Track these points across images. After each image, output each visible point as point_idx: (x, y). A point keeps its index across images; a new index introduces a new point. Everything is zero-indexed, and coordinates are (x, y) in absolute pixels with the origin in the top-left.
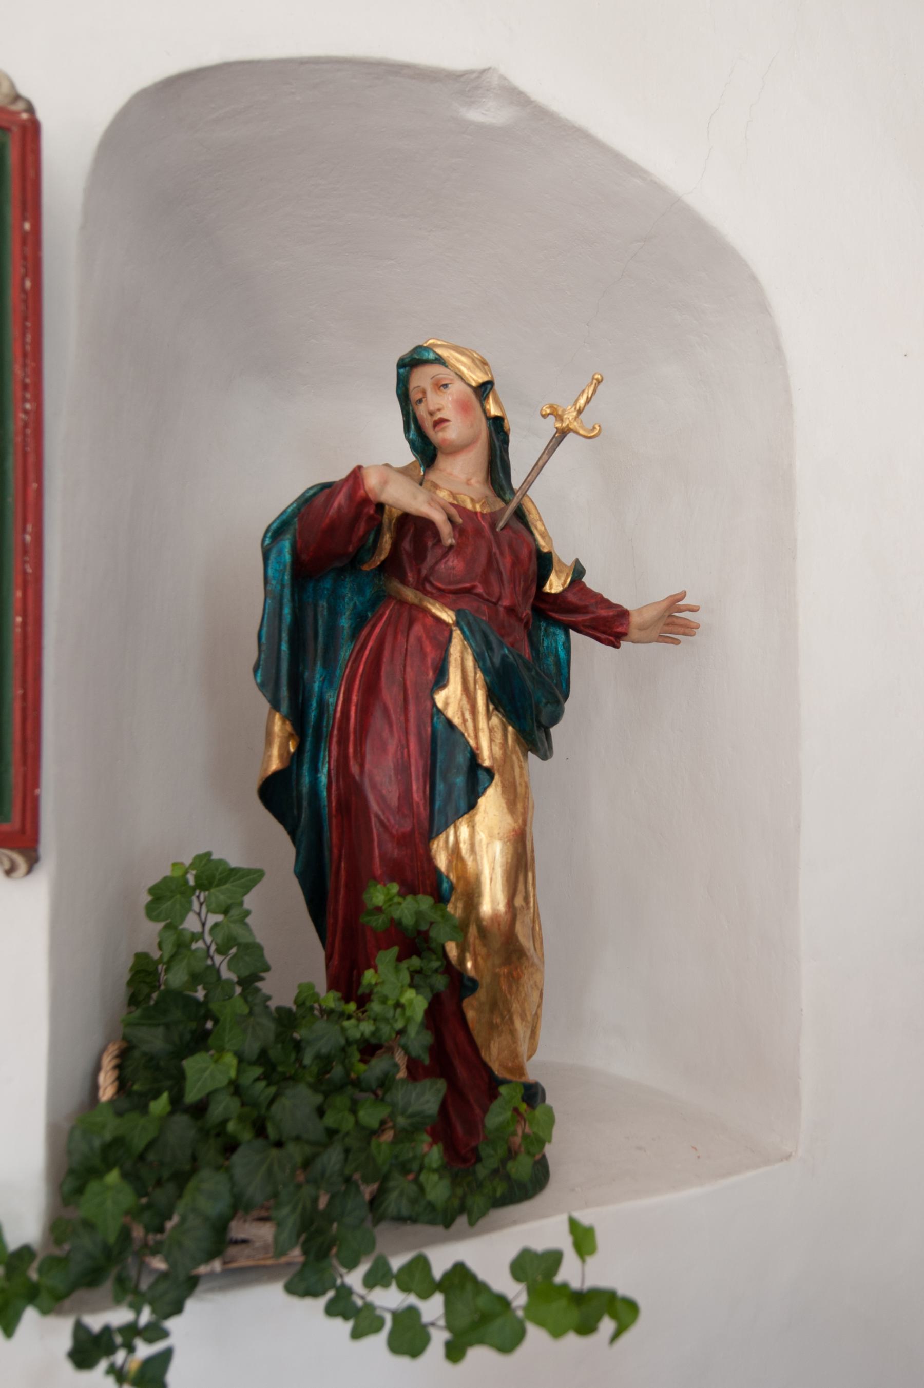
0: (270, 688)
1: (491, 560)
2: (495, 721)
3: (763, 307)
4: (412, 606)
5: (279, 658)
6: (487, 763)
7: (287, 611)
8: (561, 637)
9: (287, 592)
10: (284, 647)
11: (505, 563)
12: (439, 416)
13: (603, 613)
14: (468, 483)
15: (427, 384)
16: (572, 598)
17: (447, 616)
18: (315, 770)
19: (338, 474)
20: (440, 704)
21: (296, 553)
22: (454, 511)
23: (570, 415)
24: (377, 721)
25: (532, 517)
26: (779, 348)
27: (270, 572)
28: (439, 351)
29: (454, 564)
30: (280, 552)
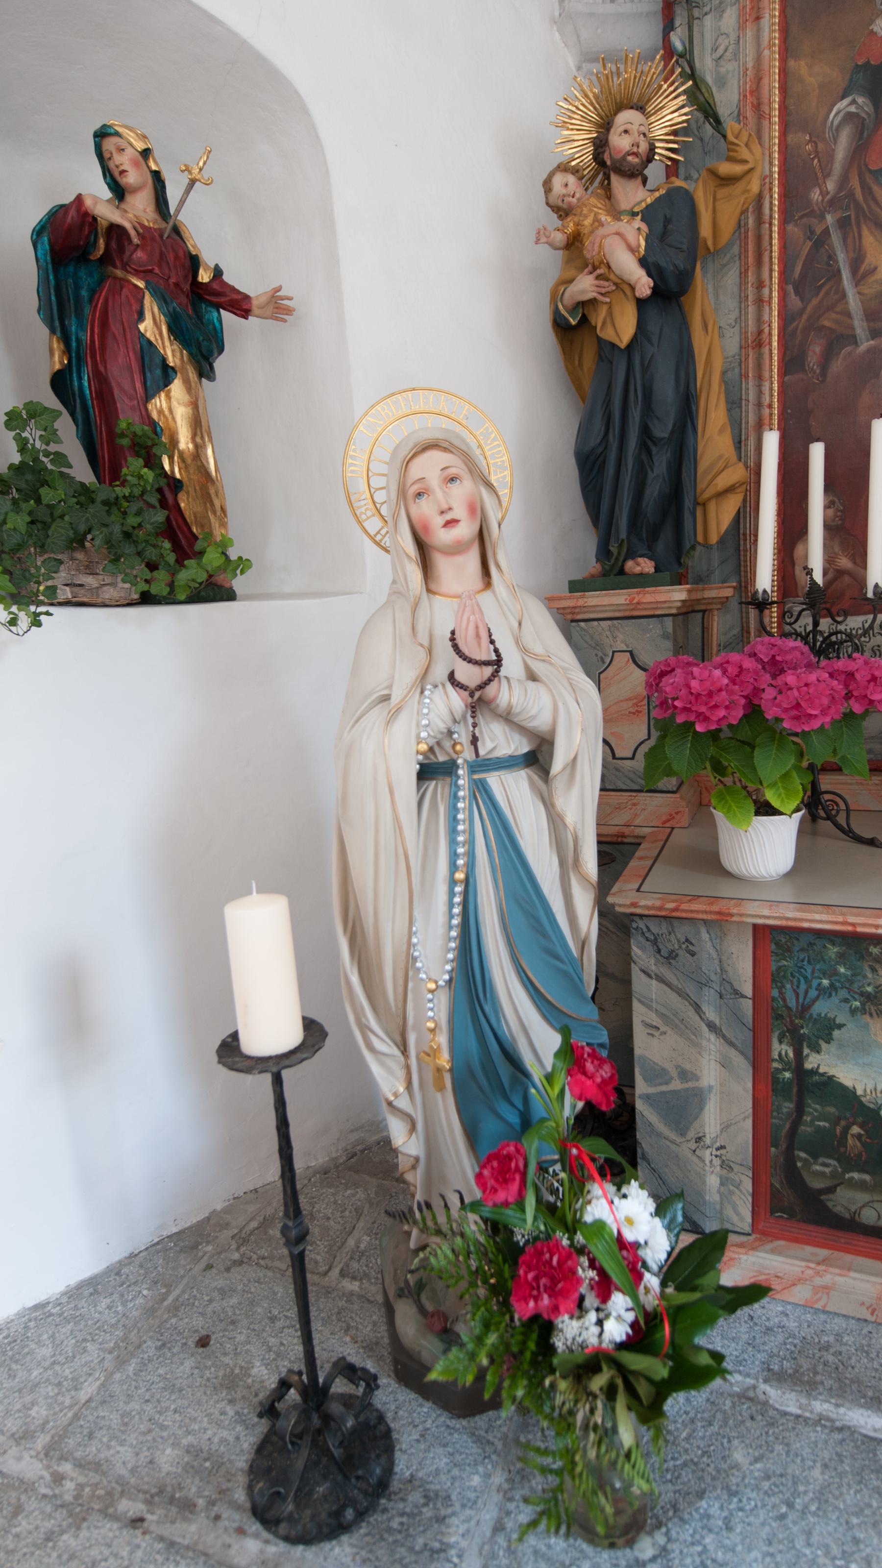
0: (50, 323)
1: (162, 254)
2: (175, 347)
3: (306, 111)
4: (121, 279)
5: (51, 304)
6: (171, 364)
7: (51, 277)
8: (215, 314)
9: (50, 266)
10: (53, 298)
11: (171, 258)
12: (122, 168)
13: (235, 297)
14: (145, 211)
15: (112, 148)
16: (215, 286)
17: (141, 284)
18: (80, 378)
19: (68, 198)
20: (142, 330)
21: (52, 250)
22: (137, 225)
23: (196, 171)
24: (110, 342)
25: (182, 229)
26: (318, 137)
27: (39, 254)
28: (117, 128)
29: (139, 254)
30: (43, 244)
